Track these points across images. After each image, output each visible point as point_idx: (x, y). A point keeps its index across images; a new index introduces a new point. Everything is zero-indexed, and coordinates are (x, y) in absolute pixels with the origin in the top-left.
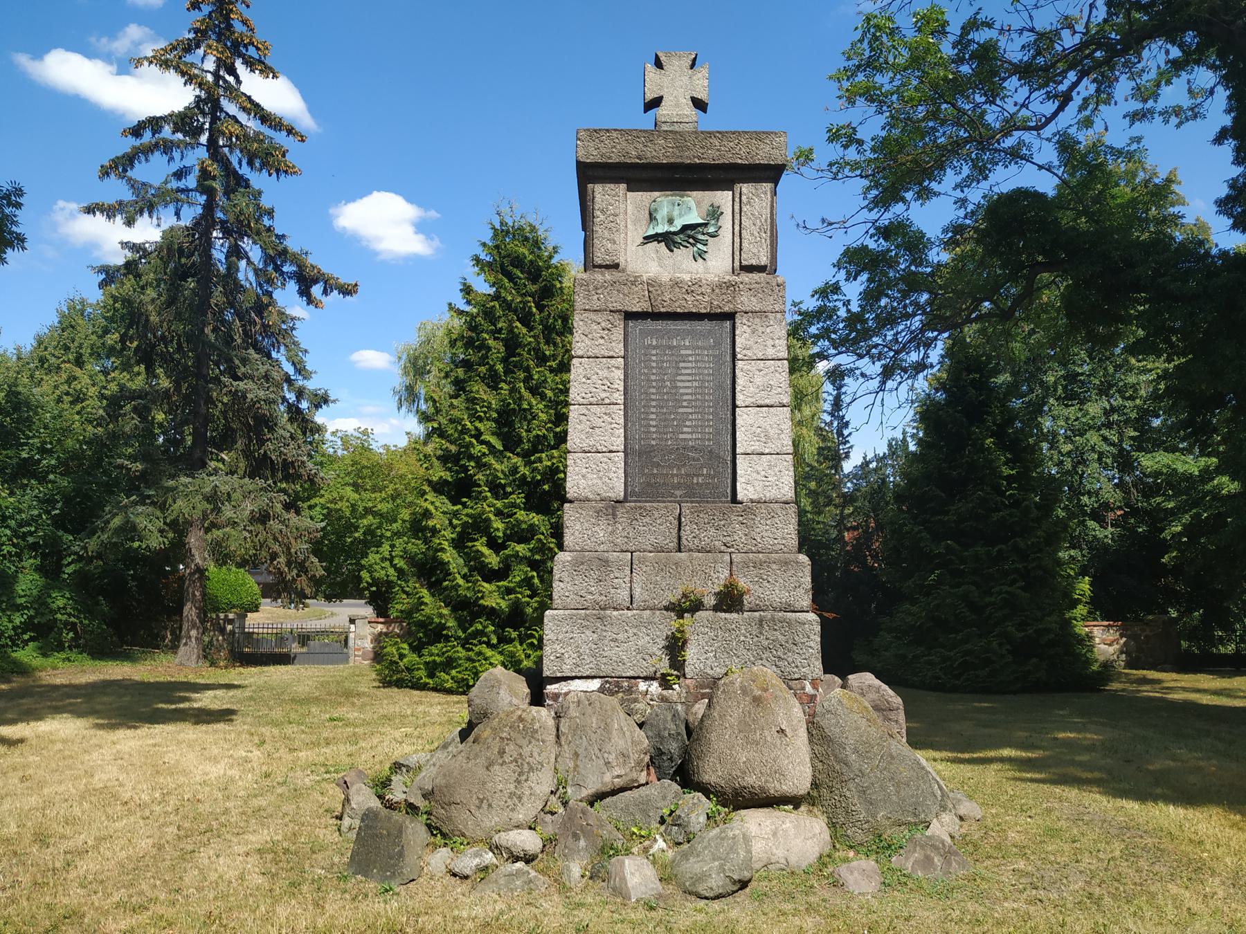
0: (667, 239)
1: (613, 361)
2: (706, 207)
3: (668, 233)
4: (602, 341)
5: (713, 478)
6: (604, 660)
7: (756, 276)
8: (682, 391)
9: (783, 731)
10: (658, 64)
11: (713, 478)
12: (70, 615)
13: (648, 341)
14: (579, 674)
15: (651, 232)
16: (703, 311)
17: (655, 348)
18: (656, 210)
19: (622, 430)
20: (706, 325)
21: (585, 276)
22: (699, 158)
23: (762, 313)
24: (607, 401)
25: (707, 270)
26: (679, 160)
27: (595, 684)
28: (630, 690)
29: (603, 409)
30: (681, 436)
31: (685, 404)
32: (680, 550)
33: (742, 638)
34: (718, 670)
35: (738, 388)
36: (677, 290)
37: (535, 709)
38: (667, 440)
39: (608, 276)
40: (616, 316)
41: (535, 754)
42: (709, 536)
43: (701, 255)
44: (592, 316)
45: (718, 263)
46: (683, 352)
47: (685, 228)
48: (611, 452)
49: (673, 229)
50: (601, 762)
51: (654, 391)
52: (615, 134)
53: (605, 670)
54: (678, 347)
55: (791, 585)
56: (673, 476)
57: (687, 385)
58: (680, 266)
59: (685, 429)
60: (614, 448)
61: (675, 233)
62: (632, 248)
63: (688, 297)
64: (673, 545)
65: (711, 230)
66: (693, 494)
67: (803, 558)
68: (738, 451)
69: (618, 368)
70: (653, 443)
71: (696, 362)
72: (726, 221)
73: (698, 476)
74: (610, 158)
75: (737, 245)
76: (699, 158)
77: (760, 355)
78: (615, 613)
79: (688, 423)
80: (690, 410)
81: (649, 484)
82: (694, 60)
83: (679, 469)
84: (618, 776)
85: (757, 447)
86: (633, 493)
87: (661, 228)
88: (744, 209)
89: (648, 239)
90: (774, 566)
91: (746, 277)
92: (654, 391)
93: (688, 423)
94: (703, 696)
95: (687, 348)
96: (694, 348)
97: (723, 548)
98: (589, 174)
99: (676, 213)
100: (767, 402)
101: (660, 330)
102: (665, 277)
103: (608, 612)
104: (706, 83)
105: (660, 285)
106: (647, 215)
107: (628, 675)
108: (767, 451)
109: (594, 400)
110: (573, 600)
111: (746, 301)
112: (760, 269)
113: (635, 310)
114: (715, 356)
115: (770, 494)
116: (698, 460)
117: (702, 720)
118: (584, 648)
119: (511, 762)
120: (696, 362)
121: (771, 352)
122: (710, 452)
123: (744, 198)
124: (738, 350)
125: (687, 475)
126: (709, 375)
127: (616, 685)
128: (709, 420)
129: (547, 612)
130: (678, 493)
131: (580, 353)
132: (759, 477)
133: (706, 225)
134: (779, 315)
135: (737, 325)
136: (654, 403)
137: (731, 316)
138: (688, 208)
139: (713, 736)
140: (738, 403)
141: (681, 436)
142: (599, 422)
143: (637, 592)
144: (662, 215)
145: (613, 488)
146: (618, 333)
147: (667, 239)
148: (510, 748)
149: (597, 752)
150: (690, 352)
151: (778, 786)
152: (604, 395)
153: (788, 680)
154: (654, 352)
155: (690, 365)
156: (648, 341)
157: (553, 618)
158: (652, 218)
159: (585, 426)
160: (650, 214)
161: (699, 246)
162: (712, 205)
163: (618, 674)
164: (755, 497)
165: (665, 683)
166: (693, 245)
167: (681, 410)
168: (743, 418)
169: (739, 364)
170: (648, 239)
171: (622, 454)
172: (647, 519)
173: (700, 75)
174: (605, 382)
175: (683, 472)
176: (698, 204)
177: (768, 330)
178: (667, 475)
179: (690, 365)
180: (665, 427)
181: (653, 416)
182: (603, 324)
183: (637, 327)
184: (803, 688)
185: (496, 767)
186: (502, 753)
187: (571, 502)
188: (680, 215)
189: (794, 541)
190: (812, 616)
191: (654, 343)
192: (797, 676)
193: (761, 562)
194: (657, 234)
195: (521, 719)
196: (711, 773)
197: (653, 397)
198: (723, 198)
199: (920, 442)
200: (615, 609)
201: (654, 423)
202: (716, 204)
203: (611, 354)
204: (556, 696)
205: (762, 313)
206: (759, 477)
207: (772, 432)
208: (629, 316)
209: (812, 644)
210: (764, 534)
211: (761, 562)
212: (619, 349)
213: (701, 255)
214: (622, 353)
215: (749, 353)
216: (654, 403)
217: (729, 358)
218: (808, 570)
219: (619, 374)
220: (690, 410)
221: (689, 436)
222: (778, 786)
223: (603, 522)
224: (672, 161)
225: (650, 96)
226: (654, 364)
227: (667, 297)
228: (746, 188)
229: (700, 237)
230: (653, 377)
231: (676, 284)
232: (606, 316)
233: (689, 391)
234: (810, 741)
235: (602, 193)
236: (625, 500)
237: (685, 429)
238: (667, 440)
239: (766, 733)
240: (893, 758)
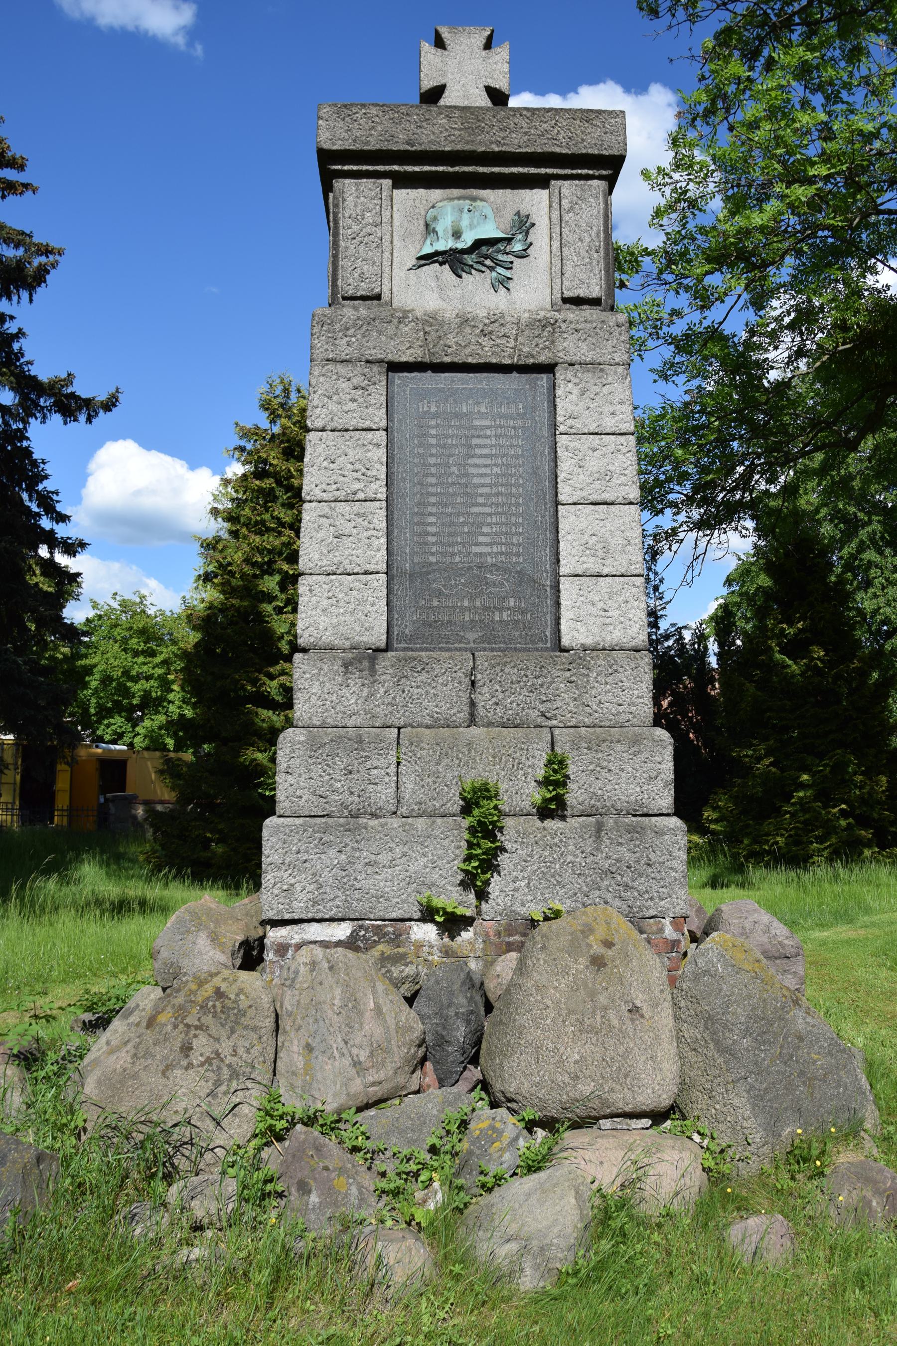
0: (454, 260)
1: (370, 435)
2: (509, 216)
3: (453, 251)
4: (352, 406)
5: (525, 612)
6: (357, 894)
7: (588, 312)
8: (476, 480)
9: (637, 1009)
10: (439, 43)
11: (525, 612)
12: (862, 548)
13: (424, 407)
14: (319, 916)
15: (428, 250)
16: (508, 361)
17: (436, 416)
18: (435, 219)
19: (383, 540)
20: (515, 380)
21: (327, 311)
22: (498, 143)
23: (594, 366)
24: (361, 496)
25: (511, 302)
26: (468, 147)
27: (342, 931)
28: (397, 939)
29: (357, 507)
30: (475, 549)
31: (481, 500)
32: (472, 721)
33: (570, 858)
34: (533, 906)
35: (561, 476)
36: (468, 330)
37: (244, 975)
38: (453, 555)
39: (363, 310)
40: (375, 368)
41: (241, 1051)
42: (515, 702)
43: (504, 282)
44: (341, 369)
45: (531, 290)
46: (477, 423)
47: (479, 244)
48: (366, 573)
49: (460, 245)
50: (347, 1061)
51: (433, 480)
52: (374, 111)
53: (358, 908)
54: (468, 415)
55: (647, 771)
56: (463, 610)
57: (483, 473)
58: (475, 294)
59: (481, 539)
60: (372, 568)
61: (464, 252)
62: (400, 273)
63: (484, 341)
64: (464, 716)
65: (518, 247)
66: (496, 640)
67: (662, 734)
68: (563, 570)
69: (378, 445)
70: (433, 559)
71: (497, 437)
72: (540, 237)
73: (501, 609)
74: (368, 143)
75: (557, 269)
76: (498, 143)
77: (592, 429)
78: (374, 823)
79: (485, 530)
80: (488, 510)
81: (425, 623)
82: (490, 39)
83: (472, 599)
84: (374, 1084)
85: (592, 565)
86: (403, 638)
87: (442, 245)
88: (566, 218)
89: (428, 259)
90: (618, 747)
91: (572, 314)
92: (433, 480)
93: (485, 530)
94: (510, 947)
95: (482, 416)
96: (494, 417)
97: (540, 720)
98: (333, 165)
99: (465, 223)
100: (607, 497)
101: (440, 390)
102: (449, 313)
103: (361, 821)
104: (506, 68)
105: (441, 324)
106: (422, 227)
107: (394, 915)
108: (605, 572)
109: (341, 494)
110: (308, 803)
111: (570, 347)
112: (595, 302)
113: (404, 359)
114: (525, 429)
115: (615, 636)
116: (502, 585)
117: (508, 990)
118: (327, 876)
119: (202, 1064)
120: (497, 437)
121: (609, 424)
122: (519, 573)
123: (565, 202)
124: (560, 419)
125: (486, 609)
126: (516, 457)
127: (374, 936)
128: (517, 525)
129: (267, 822)
130: (471, 636)
131: (320, 423)
132: (594, 611)
133: (509, 240)
134: (620, 369)
135: (558, 382)
136: (433, 500)
137: (549, 368)
138: (480, 216)
139: (525, 1020)
140: (562, 498)
141: (475, 549)
142: (348, 528)
143: (409, 787)
144: (444, 226)
145: (369, 629)
146: (378, 394)
147: (454, 260)
148: (202, 1045)
149: (342, 1044)
150: (487, 423)
151: (629, 1095)
152: (357, 486)
153: (638, 921)
154: (433, 423)
155: (488, 441)
156: (424, 407)
157: (277, 829)
158: (429, 229)
159: (327, 534)
160: (427, 225)
161: (500, 270)
162: (518, 213)
163: (379, 914)
164: (589, 641)
165: (453, 924)
166: (492, 269)
167: (475, 510)
168: (568, 519)
169: (562, 440)
170: (428, 259)
171: (383, 577)
172: (424, 677)
173: (497, 58)
174: (358, 466)
175: (477, 604)
176: (497, 212)
177: (605, 390)
178: (454, 608)
179: (488, 441)
180: (450, 534)
181: (432, 519)
182: (355, 381)
183: (399, 378)
184: (661, 930)
185: (178, 1072)
186: (187, 1049)
187: (305, 650)
188: (472, 227)
189: (646, 709)
190: (675, 822)
191: (433, 409)
192: (651, 912)
193: (603, 734)
194: (437, 253)
195: (219, 994)
196: (517, 1074)
197: (432, 490)
198: (535, 201)
199: (194, 706)
200: (374, 816)
201: (432, 529)
202: (524, 213)
203: (367, 424)
204: (282, 949)
205: (594, 366)
206: (594, 611)
207: (613, 541)
208: (394, 367)
209: (675, 864)
210: (604, 698)
211: (603, 734)
212: (379, 418)
213: (504, 282)
214: (383, 424)
215: (578, 425)
216: (433, 500)
217: (546, 432)
218: (668, 753)
219: (381, 453)
220: (488, 510)
221: (487, 549)
222: (629, 1095)
223: (355, 682)
224: (459, 147)
225: (427, 84)
226: (433, 441)
227: (451, 340)
228: (567, 188)
229: (500, 257)
230: (432, 460)
231: (465, 321)
232: (360, 368)
233: (487, 481)
234: (676, 1018)
235: (353, 193)
236: (386, 650)
237: (481, 539)
238: (453, 555)
239: (611, 1014)
240: (801, 1038)
